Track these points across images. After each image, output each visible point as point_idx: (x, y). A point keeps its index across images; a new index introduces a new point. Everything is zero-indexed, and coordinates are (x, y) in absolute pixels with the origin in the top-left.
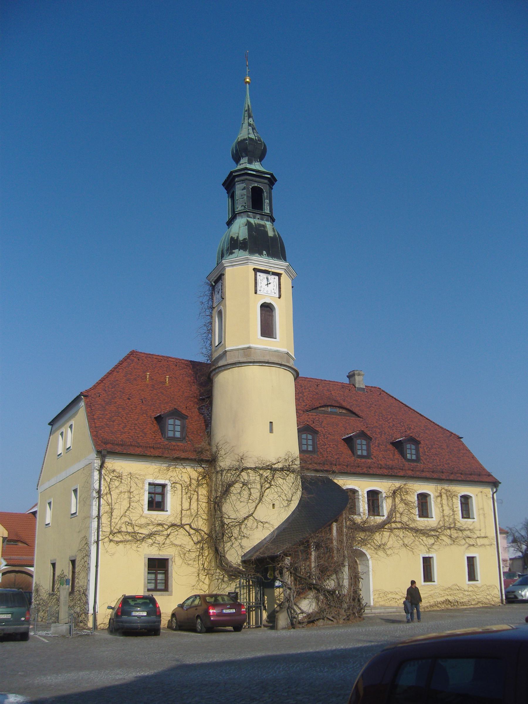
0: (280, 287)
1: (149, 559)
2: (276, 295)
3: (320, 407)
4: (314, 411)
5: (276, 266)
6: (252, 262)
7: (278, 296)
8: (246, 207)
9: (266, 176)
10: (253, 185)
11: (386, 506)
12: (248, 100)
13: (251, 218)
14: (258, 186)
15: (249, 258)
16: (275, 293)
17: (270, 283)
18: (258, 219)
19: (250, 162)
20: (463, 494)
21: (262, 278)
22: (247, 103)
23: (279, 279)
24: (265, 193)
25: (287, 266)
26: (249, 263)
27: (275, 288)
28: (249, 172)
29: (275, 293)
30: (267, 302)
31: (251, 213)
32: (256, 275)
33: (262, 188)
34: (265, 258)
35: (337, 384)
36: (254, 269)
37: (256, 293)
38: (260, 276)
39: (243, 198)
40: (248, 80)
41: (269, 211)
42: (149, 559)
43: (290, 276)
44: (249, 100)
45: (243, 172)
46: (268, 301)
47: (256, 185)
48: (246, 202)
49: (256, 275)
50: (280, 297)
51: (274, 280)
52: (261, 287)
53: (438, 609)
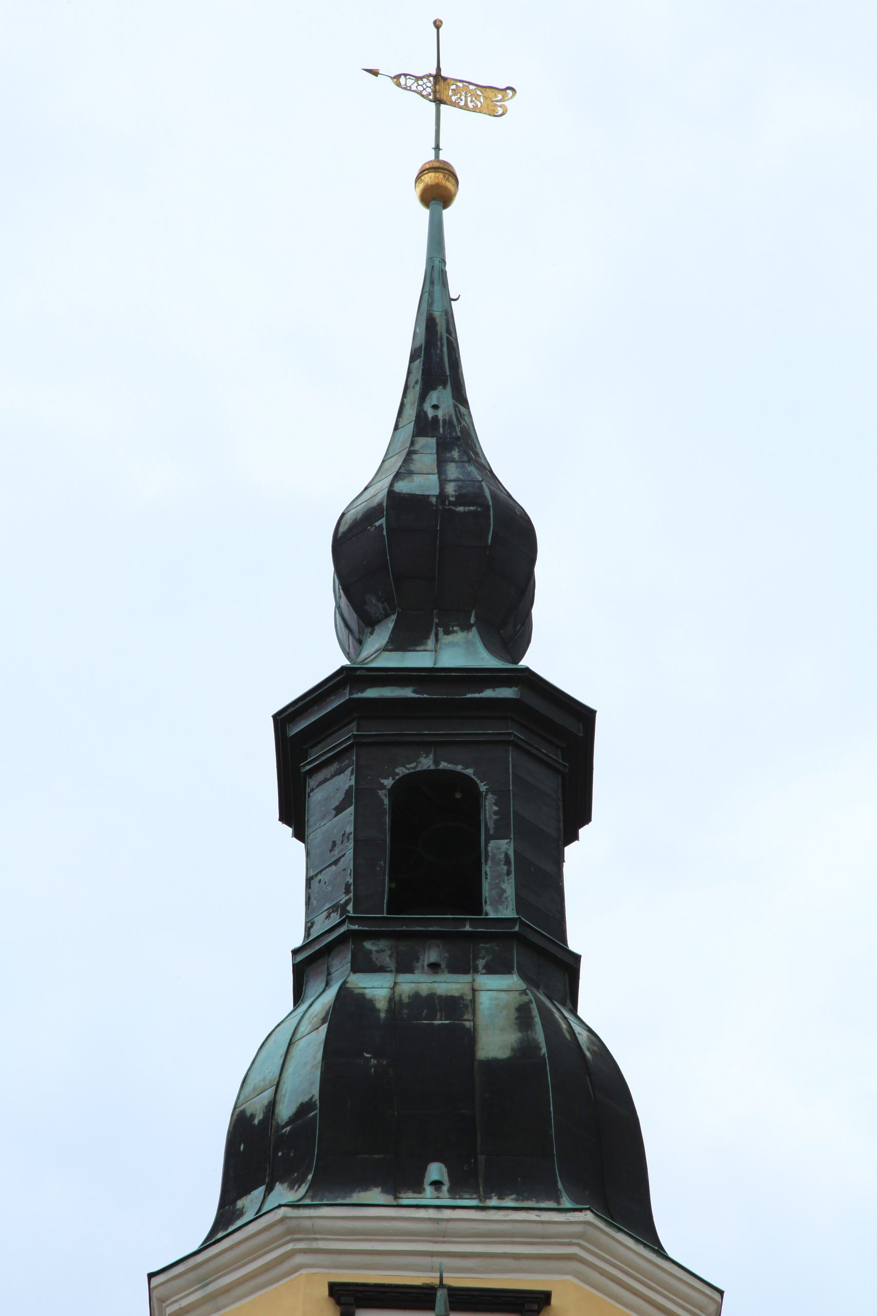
6: (322, 1245)
8: (350, 908)
9: (488, 693)
10: (401, 771)
13: (382, 969)
14: (444, 765)
15: (294, 1223)
26: (299, 1259)
28: (372, 693)
31: (383, 944)
33: (469, 772)
36: (337, 1291)
39: (335, 863)
41: (512, 904)
44: (592, 1092)
47: (426, 763)
48: (327, 881)
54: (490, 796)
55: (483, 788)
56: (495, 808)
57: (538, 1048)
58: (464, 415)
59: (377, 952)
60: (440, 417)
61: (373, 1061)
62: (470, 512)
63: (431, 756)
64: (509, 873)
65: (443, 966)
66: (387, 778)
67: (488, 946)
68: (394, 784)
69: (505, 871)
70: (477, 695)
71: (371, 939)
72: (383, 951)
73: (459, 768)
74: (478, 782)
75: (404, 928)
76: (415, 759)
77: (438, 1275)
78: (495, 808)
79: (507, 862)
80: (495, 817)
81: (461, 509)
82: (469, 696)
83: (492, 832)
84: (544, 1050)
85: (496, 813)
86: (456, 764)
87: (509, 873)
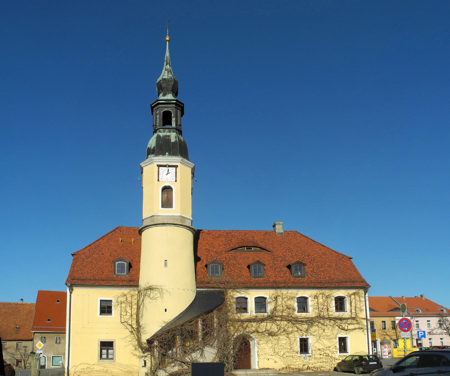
0: (158, 175)
1: (101, 342)
2: (161, 179)
3: (239, 248)
4: (234, 250)
5: (150, 162)
7: (175, 181)
10: (164, 111)
11: (270, 308)
12: (167, 53)
13: (162, 132)
14: (168, 110)
16: (173, 179)
17: (169, 173)
18: (167, 132)
19: (164, 95)
20: (300, 296)
21: (163, 170)
22: (166, 55)
23: (176, 169)
24: (173, 114)
25: (181, 160)
26: (154, 162)
27: (173, 175)
28: (160, 102)
29: (162, 179)
30: (166, 185)
31: (162, 129)
32: (159, 169)
33: (171, 111)
34: (167, 157)
35: (261, 232)
36: (158, 165)
37: (158, 181)
38: (162, 169)
40: (167, 39)
42: (101, 342)
43: (188, 166)
45: (157, 103)
46: (167, 184)
47: (166, 110)
49: (159, 169)
50: (176, 181)
51: (172, 170)
52: (163, 176)
53: (312, 371)
55: (172, 112)
73: (169, 110)
81: (170, 80)
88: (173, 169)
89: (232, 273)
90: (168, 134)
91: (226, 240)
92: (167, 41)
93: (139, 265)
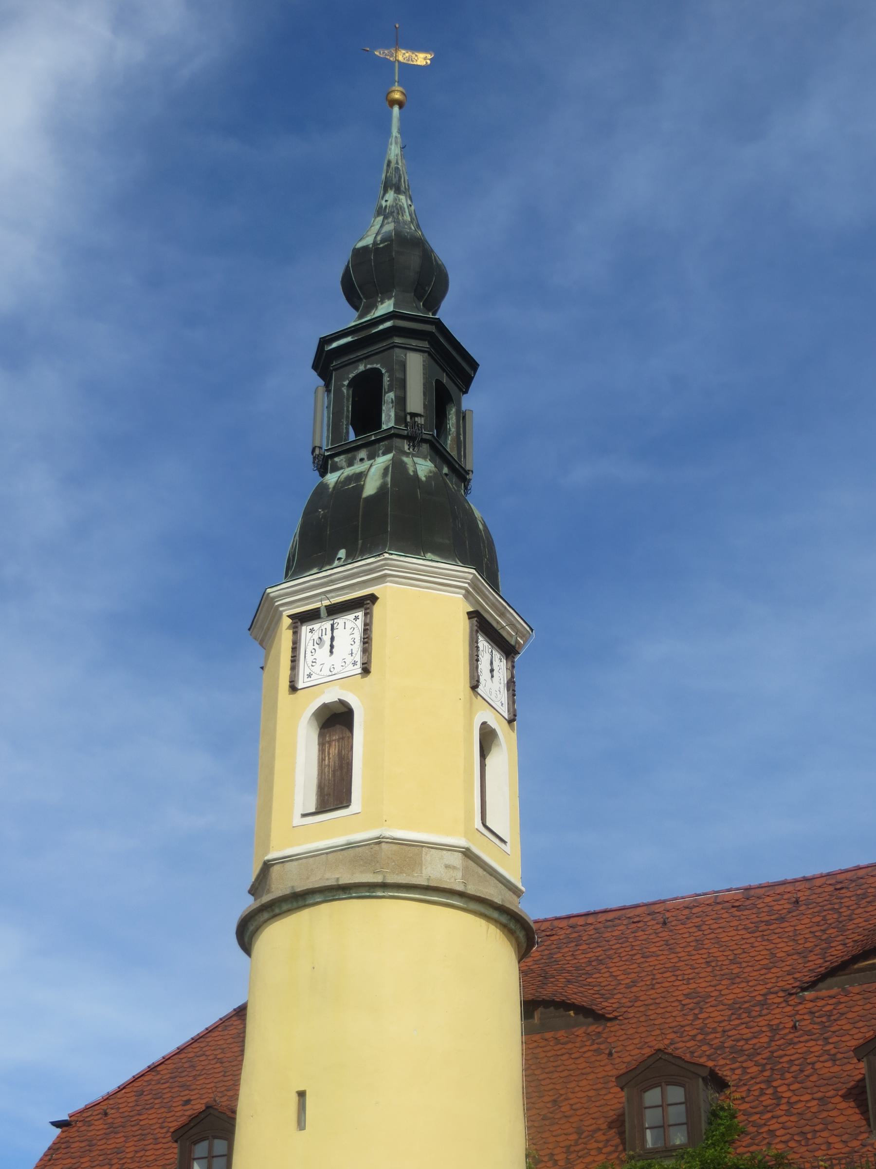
0: (292, 661)
2: (306, 679)
9: (381, 327)
10: (351, 376)
14: (369, 366)
29: (309, 676)
31: (342, 457)
40: (397, 96)
47: (361, 368)
54: (386, 374)
56: (388, 379)
57: (388, 484)
58: (401, 199)
59: (340, 461)
60: (388, 205)
61: (322, 512)
62: (385, 245)
63: (363, 365)
64: (392, 407)
65: (366, 459)
66: (345, 381)
67: (383, 443)
68: (349, 383)
69: (391, 407)
70: (376, 330)
71: (337, 457)
72: (342, 460)
74: (381, 369)
75: (348, 447)
76: (357, 368)
77: (320, 603)
78: (388, 379)
79: (392, 402)
80: (388, 383)
82: (373, 332)
83: (387, 390)
84: (389, 486)
85: (388, 381)
86: (373, 364)
87: (392, 407)
88: (356, 618)
89: (773, 1117)
90: (357, 468)
91: (813, 929)
92: (393, 103)
93: (530, 1062)
